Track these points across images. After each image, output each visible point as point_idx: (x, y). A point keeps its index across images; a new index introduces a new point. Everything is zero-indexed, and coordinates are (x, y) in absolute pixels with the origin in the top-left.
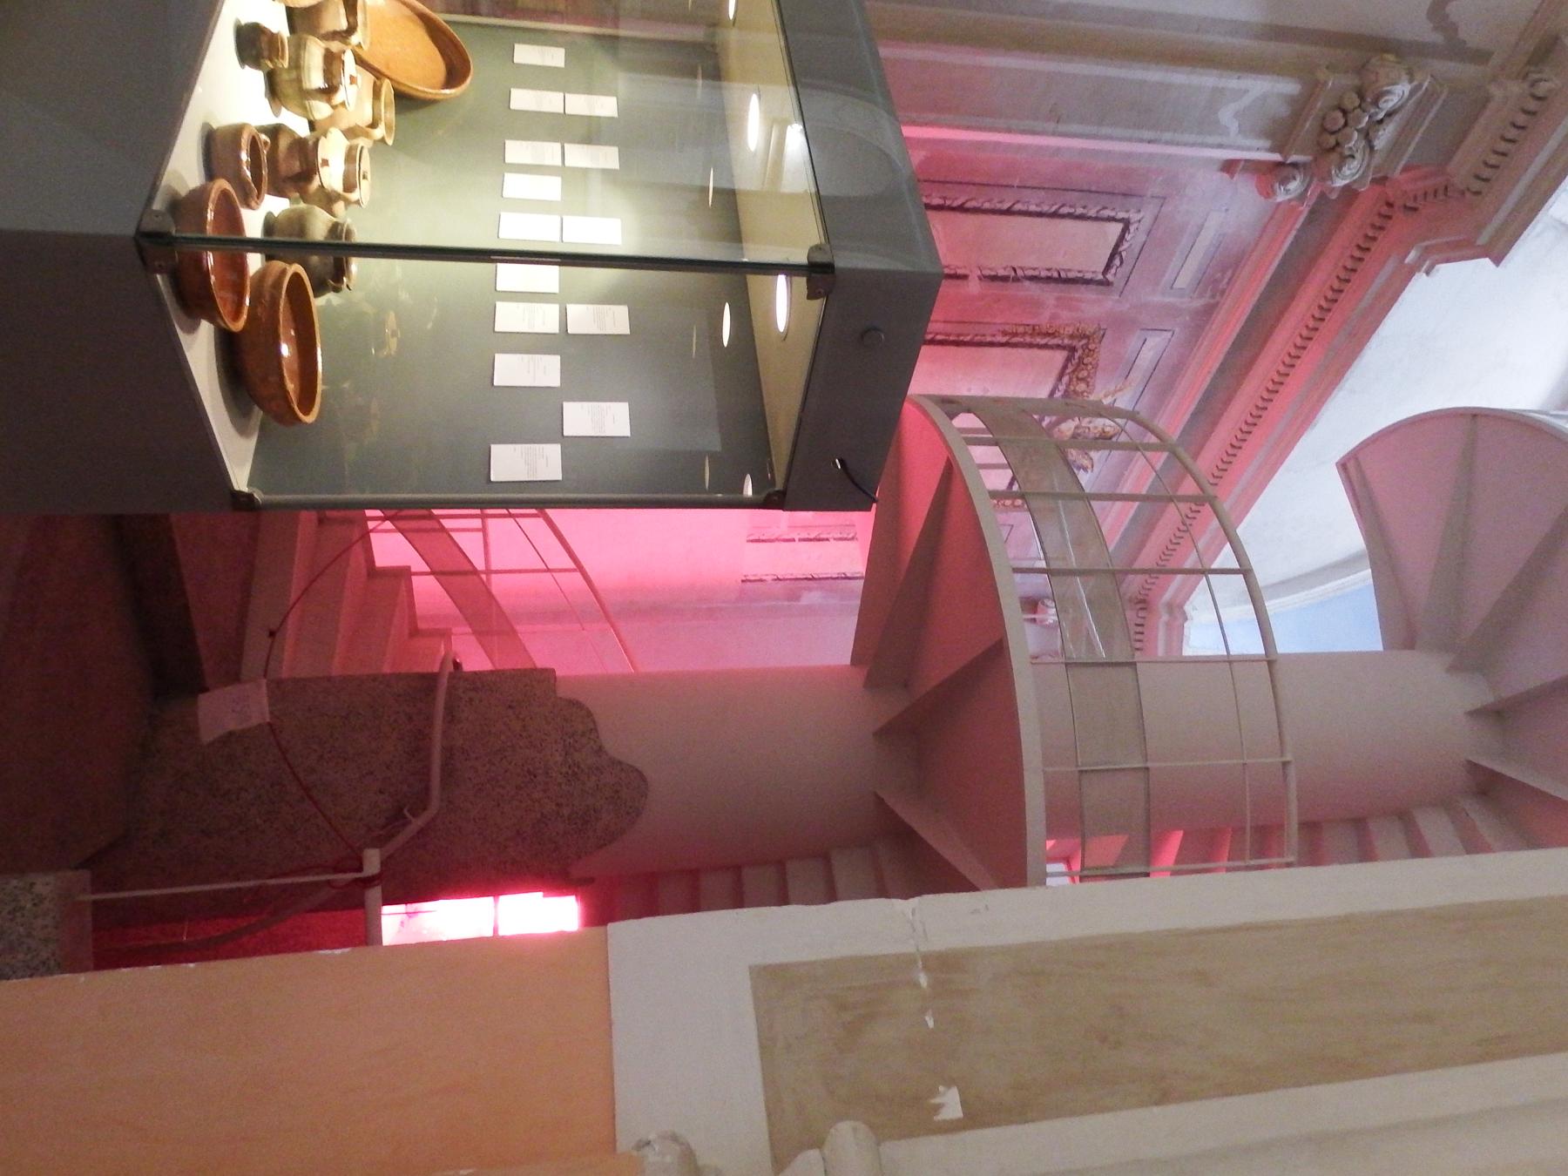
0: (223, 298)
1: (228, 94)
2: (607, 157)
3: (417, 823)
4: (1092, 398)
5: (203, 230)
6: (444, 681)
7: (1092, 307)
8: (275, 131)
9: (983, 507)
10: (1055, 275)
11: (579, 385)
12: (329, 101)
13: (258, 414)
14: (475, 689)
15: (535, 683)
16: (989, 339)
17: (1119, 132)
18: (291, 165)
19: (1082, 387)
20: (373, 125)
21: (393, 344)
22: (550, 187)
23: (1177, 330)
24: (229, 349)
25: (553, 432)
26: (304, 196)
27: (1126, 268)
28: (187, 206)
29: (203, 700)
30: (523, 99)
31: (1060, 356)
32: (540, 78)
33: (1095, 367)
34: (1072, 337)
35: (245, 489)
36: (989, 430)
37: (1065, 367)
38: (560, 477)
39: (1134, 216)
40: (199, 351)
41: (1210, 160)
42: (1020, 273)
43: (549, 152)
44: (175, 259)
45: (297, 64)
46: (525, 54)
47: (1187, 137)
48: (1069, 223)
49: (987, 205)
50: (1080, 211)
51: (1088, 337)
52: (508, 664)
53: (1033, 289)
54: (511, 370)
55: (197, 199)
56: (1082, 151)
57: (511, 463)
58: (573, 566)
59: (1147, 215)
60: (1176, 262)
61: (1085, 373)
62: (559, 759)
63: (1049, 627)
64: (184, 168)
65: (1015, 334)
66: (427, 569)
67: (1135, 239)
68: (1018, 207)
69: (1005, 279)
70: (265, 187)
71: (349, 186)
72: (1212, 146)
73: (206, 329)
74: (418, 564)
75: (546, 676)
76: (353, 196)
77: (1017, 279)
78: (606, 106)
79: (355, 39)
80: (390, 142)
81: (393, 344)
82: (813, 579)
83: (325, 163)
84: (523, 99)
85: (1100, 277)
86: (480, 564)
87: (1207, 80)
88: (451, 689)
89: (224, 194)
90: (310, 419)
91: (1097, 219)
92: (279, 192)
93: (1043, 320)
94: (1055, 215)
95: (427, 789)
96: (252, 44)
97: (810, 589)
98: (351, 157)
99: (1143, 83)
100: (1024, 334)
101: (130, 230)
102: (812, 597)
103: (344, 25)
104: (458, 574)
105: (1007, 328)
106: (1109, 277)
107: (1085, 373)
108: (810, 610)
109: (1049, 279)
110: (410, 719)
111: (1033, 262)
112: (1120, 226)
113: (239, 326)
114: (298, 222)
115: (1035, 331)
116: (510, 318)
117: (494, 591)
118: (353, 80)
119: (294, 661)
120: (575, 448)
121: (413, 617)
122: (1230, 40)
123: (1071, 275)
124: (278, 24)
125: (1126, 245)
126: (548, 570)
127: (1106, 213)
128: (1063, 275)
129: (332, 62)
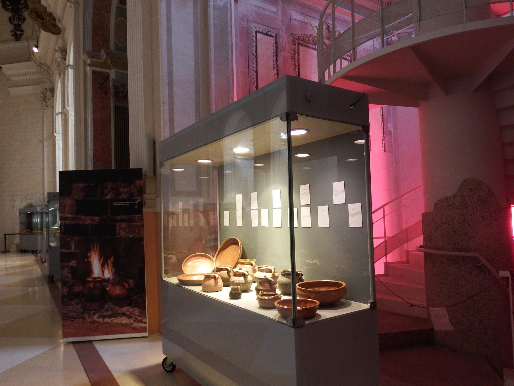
0: (309, 306)
1: (249, 301)
2: (254, 196)
3: (484, 261)
4: (315, 35)
5: (290, 309)
6: (426, 250)
7: (284, 39)
8: (258, 290)
9: (356, 64)
10: (275, 54)
11: (328, 201)
12: (247, 276)
13: (343, 300)
14: (430, 240)
15: (427, 220)
16: (297, 73)
17: (230, 39)
18: (266, 287)
19: (311, 39)
20: (252, 265)
21: (315, 261)
22: (265, 212)
23: (290, 8)
24: (324, 306)
25: (343, 207)
26: (275, 283)
27: (271, 29)
28: (284, 314)
29: (437, 328)
30: (240, 222)
31: (301, 48)
32: (233, 218)
33: (304, 35)
34: (294, 45)
35: (369, 305)
36: (329, 68)
37: (305, 46)
38: (360, 204)
39: (255, 30)
40: (326, 314)
41: (235, 7)
42: (275, 66)
43: (254, 214)
44: (300, 318)
45: (238, 284)
46: (227, 222)
47: (229, 16)
48: (258, 51)
49: (255, 80)
50: (254, 48)
51: (294, 39)
52: (420, 230)
53: (280, 60)
54: (324, 221)
55: (281, 310)
56: (236, 50)
57: (355, 218)
58: (382, 209)
59: (253, 25)
60: (267, 13)
61: (306, 39)
62: (458, 211)
63: (399, 39)
64: (273, 314)
65: (295, 64)
66: (385, 257)
67: (261, 28)
68: (255, 69)
69: (277, 71)
70: (274, 293)
71: (270, 271)
72: (231, 6)
73: (319, 312)
74: (383, 260)
75: (425, 216)
76: (273, 270)
77: (277, 67)
78: (239, 197)
79: (229, 269)
80: (256, 260)
81: (315, 261)
82: (383, 127)
83: (265, 276)
84: (240, 222)
85: (274, 38)
86: (383, 240)
87: (211, 12)
88: (430, 248)
89: (278, 303)
90: (344, 284)
91: (256, 42)
92: (275, 290)
93: (289, 55)
94: (256, 57)
95: (470, 257)
96: (235, 295)
97: (387, 127)
98: (261, 270)
99: (215, 34)
100: (295, 61)
101: (293, 329)
102: (390, 127)
103: (225, 272)
104: (389, 245)
105: (293, 68)
106: (274, 35)
107: (306, 39)
108: (395, 127)
109: (276, 55)
110: (442, 262)
111: (272, 63)
112: (258, 34)
113: (318, 303)
114: (284, 286)
115: (294, 58)
116: (306, 222)
117: (391, 236)
118: (241, 269)
119: (421, 300)
120: (349, 200)
121: (402, 262)
122: (199, 7)
123: (274, 48)
124: (228, 290)
125: (264, 31)
126: (384, 217)
127: (254, 40)
128: (275, 51)
129: (236, 275)
